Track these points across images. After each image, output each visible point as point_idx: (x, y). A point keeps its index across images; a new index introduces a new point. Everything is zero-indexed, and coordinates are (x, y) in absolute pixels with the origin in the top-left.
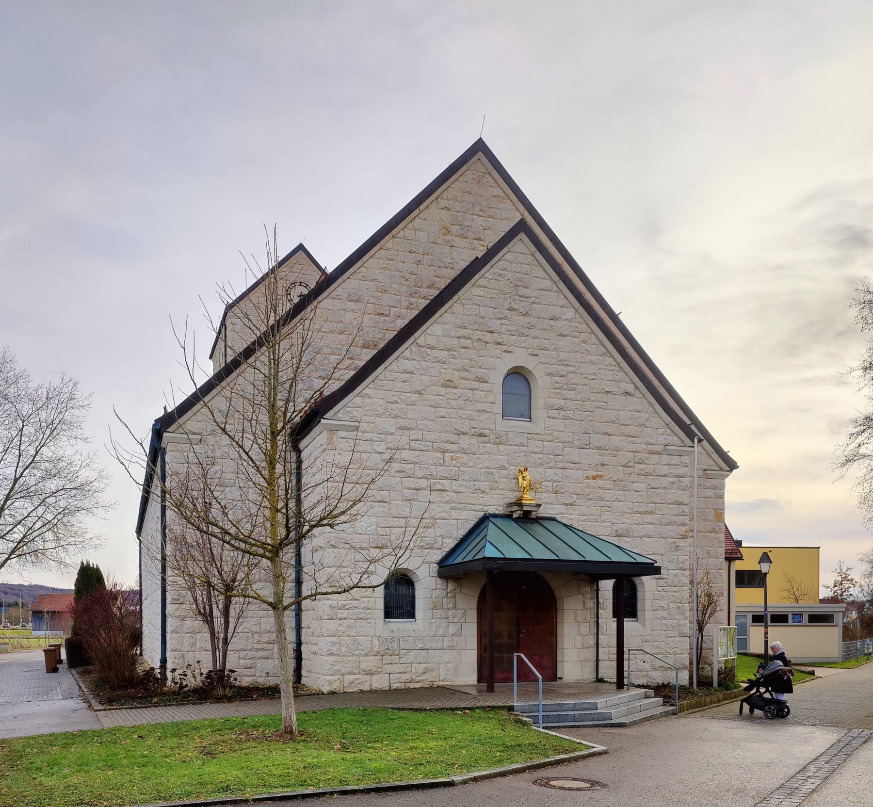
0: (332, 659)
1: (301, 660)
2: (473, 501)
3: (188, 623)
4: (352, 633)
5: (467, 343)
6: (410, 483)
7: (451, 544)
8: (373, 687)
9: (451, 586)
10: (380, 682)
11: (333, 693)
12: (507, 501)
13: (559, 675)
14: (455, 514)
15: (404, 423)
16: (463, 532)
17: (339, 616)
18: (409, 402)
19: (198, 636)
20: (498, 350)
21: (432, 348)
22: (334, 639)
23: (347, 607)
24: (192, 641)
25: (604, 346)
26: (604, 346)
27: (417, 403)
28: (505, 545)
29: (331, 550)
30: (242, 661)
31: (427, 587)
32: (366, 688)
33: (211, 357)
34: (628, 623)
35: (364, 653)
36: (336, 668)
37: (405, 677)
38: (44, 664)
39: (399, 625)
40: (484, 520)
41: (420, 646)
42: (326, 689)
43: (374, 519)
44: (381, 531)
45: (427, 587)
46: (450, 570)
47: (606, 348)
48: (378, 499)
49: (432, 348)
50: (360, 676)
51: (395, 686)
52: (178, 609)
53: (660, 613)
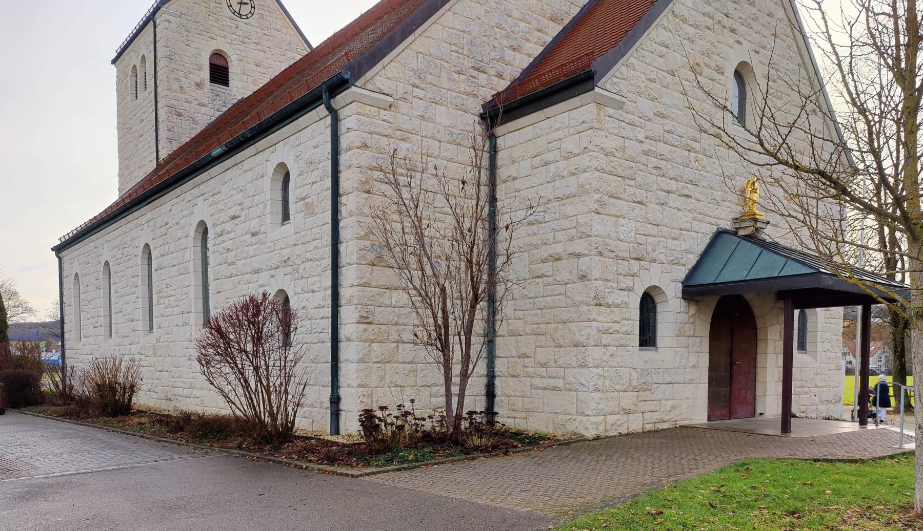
0: (596, 395)
1: (494, 396)
2: (709, 213)
3: (407, 351)
4: (614, 364)
5: (710, 22)
6: (665, 183)
7: (693, 260)
8: (631, 430)
9: (693, 310)
10: (635, 424)
11: (598, 438)
12: (734, 215)
13: (758, 411)
14: (697, 226)
15: (661, 109)
16: (702, 248)
17: (604, 341)
18: (665, 84)
19: (388, 366)
20: (730, 38)
21: (685, 21)
22: (599, 371)
23: (611, 331)
24: (382, 373)
25: (801, 55)
26: (801, 55)
27: (671, 87)
28: (738, 268)
29: (597, 258)
30: (433, 399)
31: (673, 312)
32: (625, 431)
33: (114, 62)
34: (798, 357)
35: (624, 387)
36: (601, 407)
37: (655, 416)
38: (780, 420)
39: (648, 354)
40: (720, 234)
41: (668, 379)
42: (590, 434)
43: (633, 223)
44: (641, 239)
45: (673, 312)
46: (692, 292)
47: (802, 59)
48: (638, 199)
49: (685, 21)
50: (619, 416)
51: (648, 427)
52: (365, 330)
53: (827, 346)
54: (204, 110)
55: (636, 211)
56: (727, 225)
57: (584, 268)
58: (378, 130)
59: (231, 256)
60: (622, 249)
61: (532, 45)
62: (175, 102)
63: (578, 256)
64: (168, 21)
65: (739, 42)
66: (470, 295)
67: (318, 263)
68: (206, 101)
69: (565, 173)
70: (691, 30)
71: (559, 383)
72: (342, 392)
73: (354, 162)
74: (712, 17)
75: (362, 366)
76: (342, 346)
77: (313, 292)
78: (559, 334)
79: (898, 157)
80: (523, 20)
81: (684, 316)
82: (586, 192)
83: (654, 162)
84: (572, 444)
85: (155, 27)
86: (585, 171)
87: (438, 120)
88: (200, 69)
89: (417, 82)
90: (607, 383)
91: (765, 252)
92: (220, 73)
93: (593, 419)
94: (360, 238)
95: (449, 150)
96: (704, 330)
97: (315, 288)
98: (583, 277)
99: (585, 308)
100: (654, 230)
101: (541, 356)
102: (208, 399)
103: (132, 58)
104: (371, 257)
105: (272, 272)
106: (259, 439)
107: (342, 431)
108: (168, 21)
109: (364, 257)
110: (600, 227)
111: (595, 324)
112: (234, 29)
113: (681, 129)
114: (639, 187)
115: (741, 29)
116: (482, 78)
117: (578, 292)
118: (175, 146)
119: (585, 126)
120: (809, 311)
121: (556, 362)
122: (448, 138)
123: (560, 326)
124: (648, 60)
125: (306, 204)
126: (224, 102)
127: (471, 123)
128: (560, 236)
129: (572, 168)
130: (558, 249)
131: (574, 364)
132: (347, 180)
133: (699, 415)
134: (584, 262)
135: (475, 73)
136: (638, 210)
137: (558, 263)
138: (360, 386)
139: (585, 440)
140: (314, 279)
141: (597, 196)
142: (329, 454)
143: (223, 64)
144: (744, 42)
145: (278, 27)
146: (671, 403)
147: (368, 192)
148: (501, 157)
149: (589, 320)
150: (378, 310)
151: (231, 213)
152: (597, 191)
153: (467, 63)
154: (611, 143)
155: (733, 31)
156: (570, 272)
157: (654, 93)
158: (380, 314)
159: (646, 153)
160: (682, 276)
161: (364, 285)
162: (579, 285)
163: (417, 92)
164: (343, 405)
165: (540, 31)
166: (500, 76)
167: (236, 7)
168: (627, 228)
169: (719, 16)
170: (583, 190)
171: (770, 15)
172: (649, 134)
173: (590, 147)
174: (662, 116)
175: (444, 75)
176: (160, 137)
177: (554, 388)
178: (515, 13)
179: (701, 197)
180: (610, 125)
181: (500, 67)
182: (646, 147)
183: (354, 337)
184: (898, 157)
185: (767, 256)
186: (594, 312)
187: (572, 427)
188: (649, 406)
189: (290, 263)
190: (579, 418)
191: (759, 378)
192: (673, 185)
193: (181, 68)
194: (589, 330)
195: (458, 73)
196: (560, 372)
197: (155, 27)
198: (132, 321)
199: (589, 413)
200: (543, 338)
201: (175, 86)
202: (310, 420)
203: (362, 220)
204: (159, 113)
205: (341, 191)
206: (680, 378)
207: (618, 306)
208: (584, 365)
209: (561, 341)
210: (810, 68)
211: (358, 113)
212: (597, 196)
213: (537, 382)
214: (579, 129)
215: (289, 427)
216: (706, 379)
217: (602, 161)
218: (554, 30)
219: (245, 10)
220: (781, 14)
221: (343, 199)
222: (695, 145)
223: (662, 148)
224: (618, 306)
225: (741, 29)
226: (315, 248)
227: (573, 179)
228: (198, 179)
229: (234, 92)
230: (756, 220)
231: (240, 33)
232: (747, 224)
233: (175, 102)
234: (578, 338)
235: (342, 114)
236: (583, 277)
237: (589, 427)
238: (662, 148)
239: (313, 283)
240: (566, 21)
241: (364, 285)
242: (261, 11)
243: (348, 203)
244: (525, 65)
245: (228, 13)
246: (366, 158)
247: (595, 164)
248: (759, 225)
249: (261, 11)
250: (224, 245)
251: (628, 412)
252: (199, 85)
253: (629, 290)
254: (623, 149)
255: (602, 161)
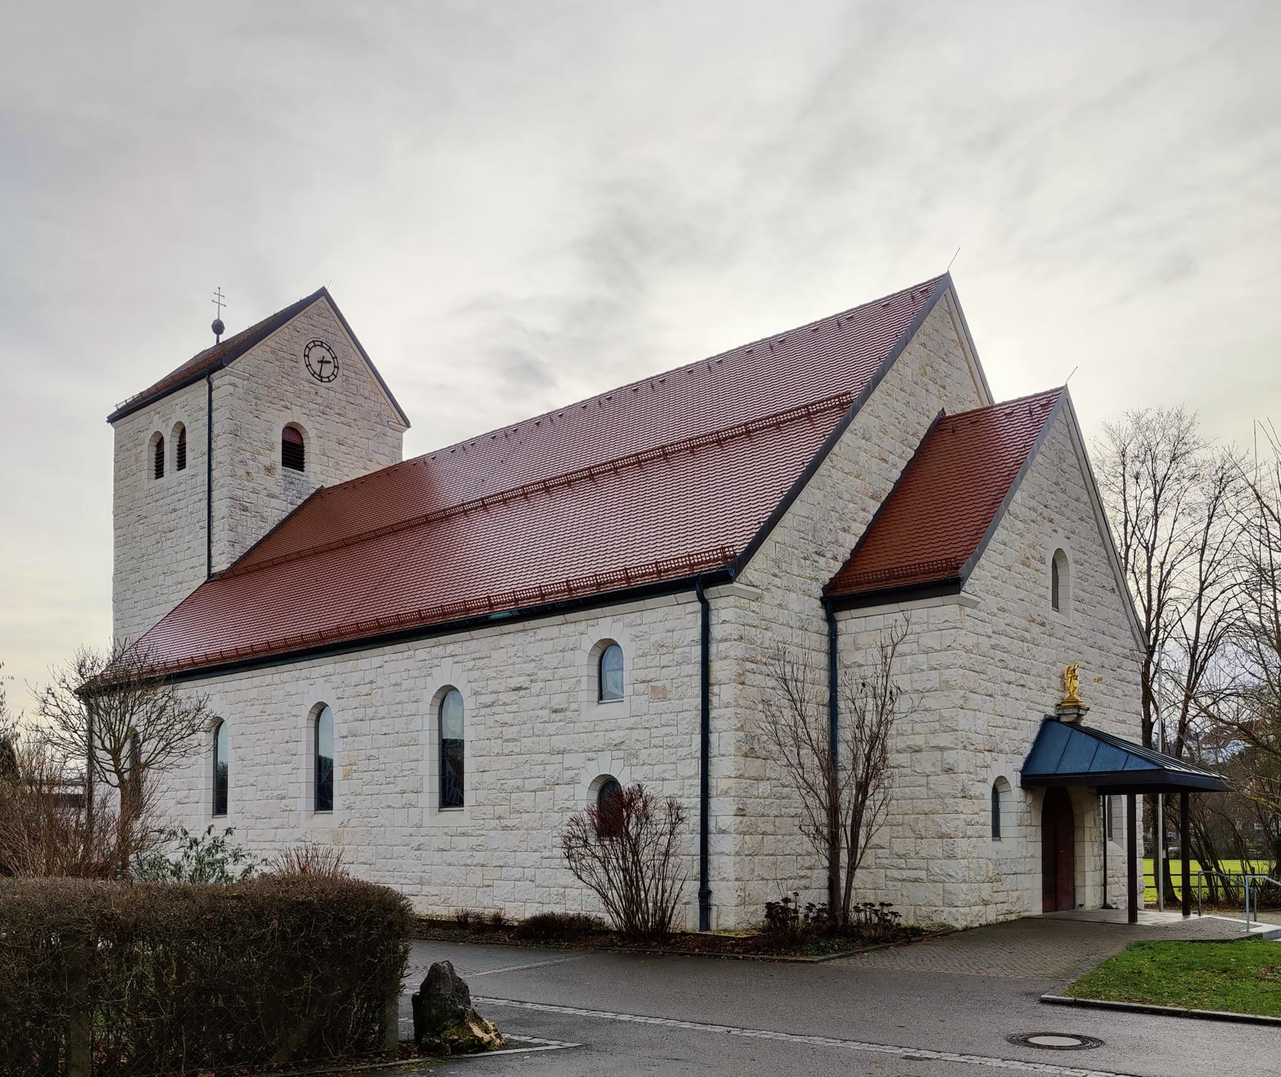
0: (964, 886)
11: (966, 929)
12: (1056, 702)
13: (1078, 902)
19: (756, 859)
20: (1048, 527)
21: (1016, 517)
28: (1077, 761)
32: (984, 923)
33: (113, 419)
37: (1006, 907)
40: (1047, 722)
42: (960, 925)
45: (1015, 798)
51: (1001, 918)
54: (274, 502)
55: (988, 704)
56: (1051, 712)
57: (951, 762)
58: (750, 622)
59: (509, 732)
60: (979, 741)
61: (857, 524)
62: (240, 493)
63: (942, 749)
64: (234, 385)
65: (1055, 531)
66: (846, 788)
67: (673, 751)
68: (277, 491)
69: (925, 667)
70: (1020, 525)
71: (922, 874)
72: (712, 885)
73: (732, 653)
74: (1035, 511)
75: (738, 859)
76: (713, 839)
77: (664, 780)
78: (920, 825)
79: (1150, 601)
80: (852, 501)
81: (1024, 805)
82: (951, 688)
83: (999, 655)
84: (945, 934)
85: (211, 390)
86: (948, 667)
87: (791, 606)
88: (271, 449)
89: (777, 571)
90: (972, 875)
91: (1103, 744)
92: (293, 454)
93: (962, 910)
94: (737, 730)
95: (798, 636)
96: (1037, 820)
97: (666, 776)
98: (949, 770)
99: (952, 801)
100: (1000, 721)
101: (899, 847)
102: (579, 898)
103: (159, 420)
104: (745, 748)
105: (590, 755)
106: (644, 939)
107: (713, 926)
108: (234, 385)
109: (740, 748)
110: (964, 721)
111: (962, 816)
112: (313, 396)
113: (1017, 621)
114: (989, 680)
115: (1056, 517)
116: (822, 560)
117: (943, 783)
118: (239, 551)
119: (947, 624)
120: (1113, 797)
121: (917, 853)
122: (798, 624)
123: (922, 817)
124: (993, 559)
125: (653, 687)
126: (299, 492)
127: (815, 609)
128: (918, 728)
129: (934, 663)
130: (919, 741)
131: (939, 855)
132: (719, 670)
133: (1037, 909)
134: (950, 757)
135: (817, 557)
136: (989, 703)
137: (917, 755)
138: (737, 879)
139: (957, 931)
140: (664, 767)
141: (962, 692)
142: (709, 948)
143: (297, 441)
144: (1059, 530)
145: (367, 394)
146: (1016, 894)
147: (743, 683)
148: (842, 641)
149: (956, 812)
150: (750, 801)
151: (514, 683)
152: (962, 687)
153: (812, 548)
154: (969, 641)
155: (1051, 521)
156: (934, 765)
157: (997, 590)
158: (752, 805)
159: (993, 647)
160: (1020, 765)
161: (741, 776)
162: (944, 777)
163: (777, 581)
164: (715, 899)
165: (864, 510)
166: (835, 558)
167: (316, 367)
168: (982, 720)
169: (1041, 508)
170: (947, 686)
171: (1077, 500)
172: (995, 629)
173: (954, 645)
174: (1002, 610)
175: (795, 562)
176: (215, 538)
177: (916, 880)
178: (846, 496)
179: (1033, 686)
180: (969, 623)
181: (835, 548)
182: (993, 642)
183: (732, 829)
184: (1150, 601)
185: (1105, 750)
186: (963, 805)
187: (937, 919)
188: (999, 897)
189: (623, 747)
190: (947, 909)
191: (1078, 867)
192: (1012, 676)
193: (248, 447)
194: (956, 823)
195: (805, 558)
196: (923, 864)
197: (211, 390)
198: (283, 798)
199: (959, 904)
200: (900, 829)
201: (241, 471)
202: (686, 919)
203: (739, 711)
204: (215, 505)
205: (712, 680)
206: (1021, 869)
207: (977, 798)
208: (952, 857)
209: (923, 832)
210: (1110, 548)
211: (736, 607)
212: (962, 692)
213: (896, 874)
214: (941, 627)
215: (663, 923)
216: (1039, 869)
217: (964, 659)
218: (874, 507)
219: (327, 370)
220: (1085, 498)
221: (715, 689)
222: (1027, 635)
223: (1004, 641)
224: (977, 798)
225: (1056, 517)
226: (666, 735)
227: (934, 674)
228: (443, 639)
229: (312, 479)
230: (1079, 708)
231: (319, 400)
232: (1071, 711)
233: (240, 493)
234: (944, 829)
235: (713, 604)
236: (949, 770)
237: (960, 918)
238: (1004, 641)
239: (664, 771)
240: (883, 498)
241: (741, 776)
242: (346, 372)
243: (723, 694)
244: (853, 546)
245: (305, 373)
246: (737, 650)
247: (960, 662)
248: (1081, 712)
249: (346, 372)
250: (497, 718)
251: (986, 903)
252: (269, 470)
253: (984, 781)
254: (977, 645)
255: (964, 659)
